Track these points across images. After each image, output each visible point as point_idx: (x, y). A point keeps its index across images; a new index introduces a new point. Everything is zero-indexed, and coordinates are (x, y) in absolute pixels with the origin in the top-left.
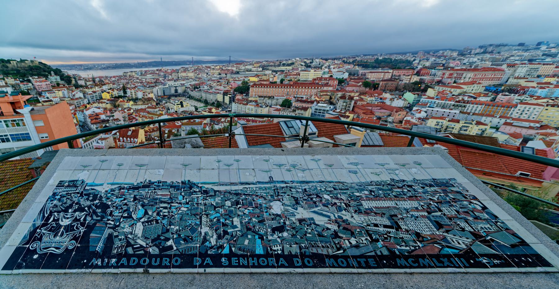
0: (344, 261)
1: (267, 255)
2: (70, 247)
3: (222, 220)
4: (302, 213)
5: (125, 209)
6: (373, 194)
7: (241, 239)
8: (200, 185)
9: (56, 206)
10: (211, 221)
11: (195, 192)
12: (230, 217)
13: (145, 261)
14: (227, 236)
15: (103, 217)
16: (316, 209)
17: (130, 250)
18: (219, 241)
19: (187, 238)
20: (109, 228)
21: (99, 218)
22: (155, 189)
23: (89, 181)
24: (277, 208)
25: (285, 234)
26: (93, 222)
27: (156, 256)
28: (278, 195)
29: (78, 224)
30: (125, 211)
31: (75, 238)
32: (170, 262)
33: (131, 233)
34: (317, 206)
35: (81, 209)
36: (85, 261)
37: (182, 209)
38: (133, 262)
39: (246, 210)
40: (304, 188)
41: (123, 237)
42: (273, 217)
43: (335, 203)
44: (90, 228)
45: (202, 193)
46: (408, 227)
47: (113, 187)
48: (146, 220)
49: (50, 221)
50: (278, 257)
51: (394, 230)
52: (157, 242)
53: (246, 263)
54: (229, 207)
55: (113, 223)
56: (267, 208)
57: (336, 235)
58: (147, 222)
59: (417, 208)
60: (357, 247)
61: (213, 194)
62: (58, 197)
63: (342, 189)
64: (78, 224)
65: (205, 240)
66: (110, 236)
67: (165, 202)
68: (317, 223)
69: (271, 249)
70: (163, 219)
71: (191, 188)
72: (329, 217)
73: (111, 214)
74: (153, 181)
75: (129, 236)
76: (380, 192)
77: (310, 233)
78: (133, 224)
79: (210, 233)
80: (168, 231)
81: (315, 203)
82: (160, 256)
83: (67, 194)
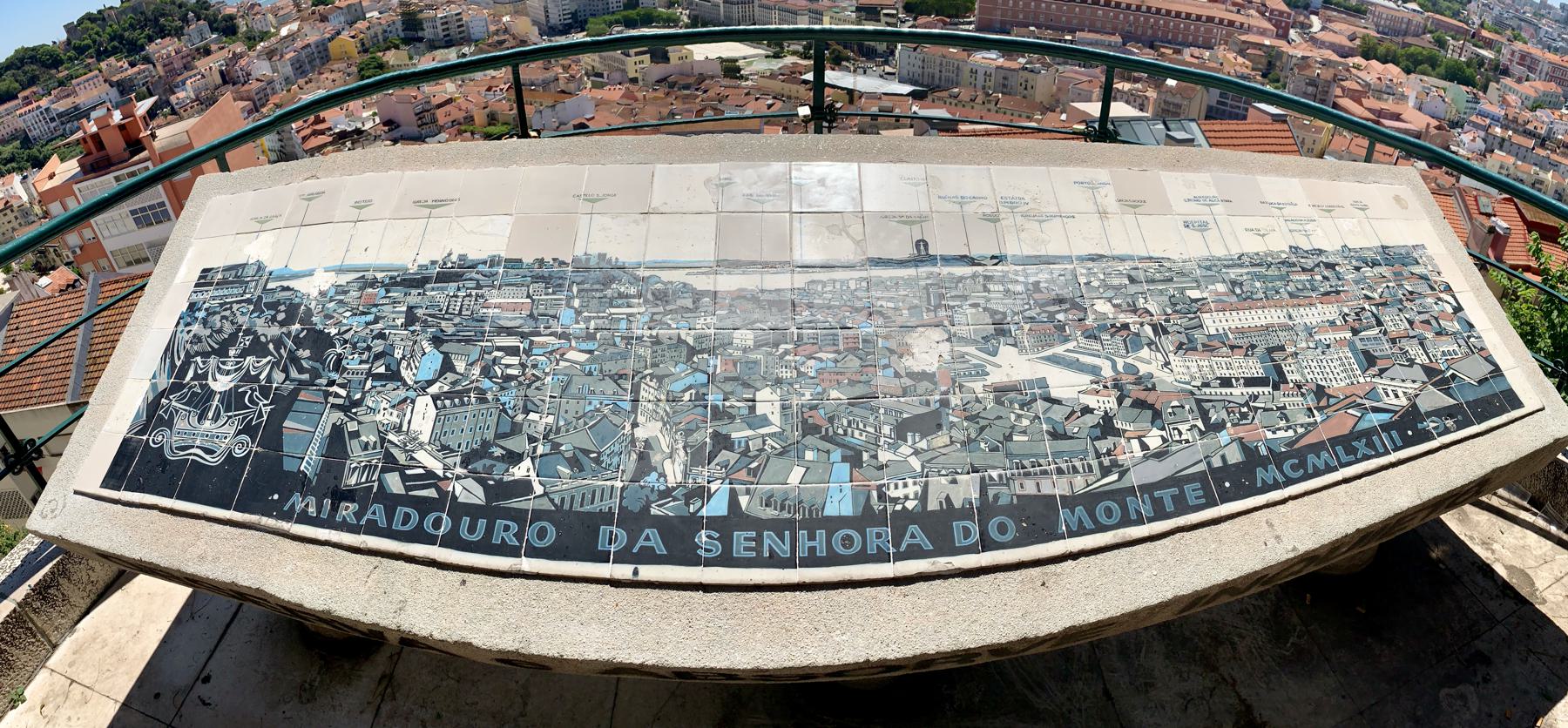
0: (1114, 506)
1: (866, 518)
2: (239, 453)
3: (714, 398)
4: (1013, 365)
5: (380, 349)
6: (1238, 291)
7: (775, 464)
8: (641, 273)
9: (197, 339)
10: (673, 399)
11: (621, 295)
12: (746, 385)
13: (437, 523)
14: (724, 455)
15: (316, 374)
16: (1059, 350)
17: (394, 483)
18: (695, 470)
19: (580, 456)
20: (333, 406)
21: (306, 377)
22: (479, 287)
23: (273, 265)
24: (927, 352)
25: (941, 439)
26: (290, 386)
27: (473, 511)
28: (938, 306)
29: (253, 390)
30: (378, 357)
31: (248, 429)
32: (519, 536)
33: (398, 429)
34: (1066, 340)
35: (257, 348)
36: (276, 497)
37: (572, 355)
38: (404, 524)
39: (811, 363)
40: (1032, 279)
41: (373, 439)
42: (907, 382)
43: (1126, 326)
44: (284, 404)
45: (646, 301)
46: (1303, 375)
47: (343, 279)
48: (446, 388)
49: (188, 378)
50: (903, 519)
51: (1267, 390)
52: (478, 465)
53: (784, 549)
54: (745, 350)
55: (343, 392)
56: (892, 352)
57: (1107, 427)
58: (449, 395)
59: (1332, 323)
60: (1160, 455)
61: (688, 303)
62: (201, 315)
63: (1153, 281)
64: (253, 390)
65: (644, 463)
66: (337, 431)
67: (509, 331)
68: (1054, 394)
69: (882, 497)
70: (503, 389)
71: (607, 282)
72: (1094, 370)
73: (338, 366)
74: (473, 256)
75: (391, 437)
76: (1258, 285)
77: (1024, 432)
78: (405, 400)
79: (664, 441)
80: (516, 429)
81: (1061, 327)
82: (487, 512)
83: (221, 305)
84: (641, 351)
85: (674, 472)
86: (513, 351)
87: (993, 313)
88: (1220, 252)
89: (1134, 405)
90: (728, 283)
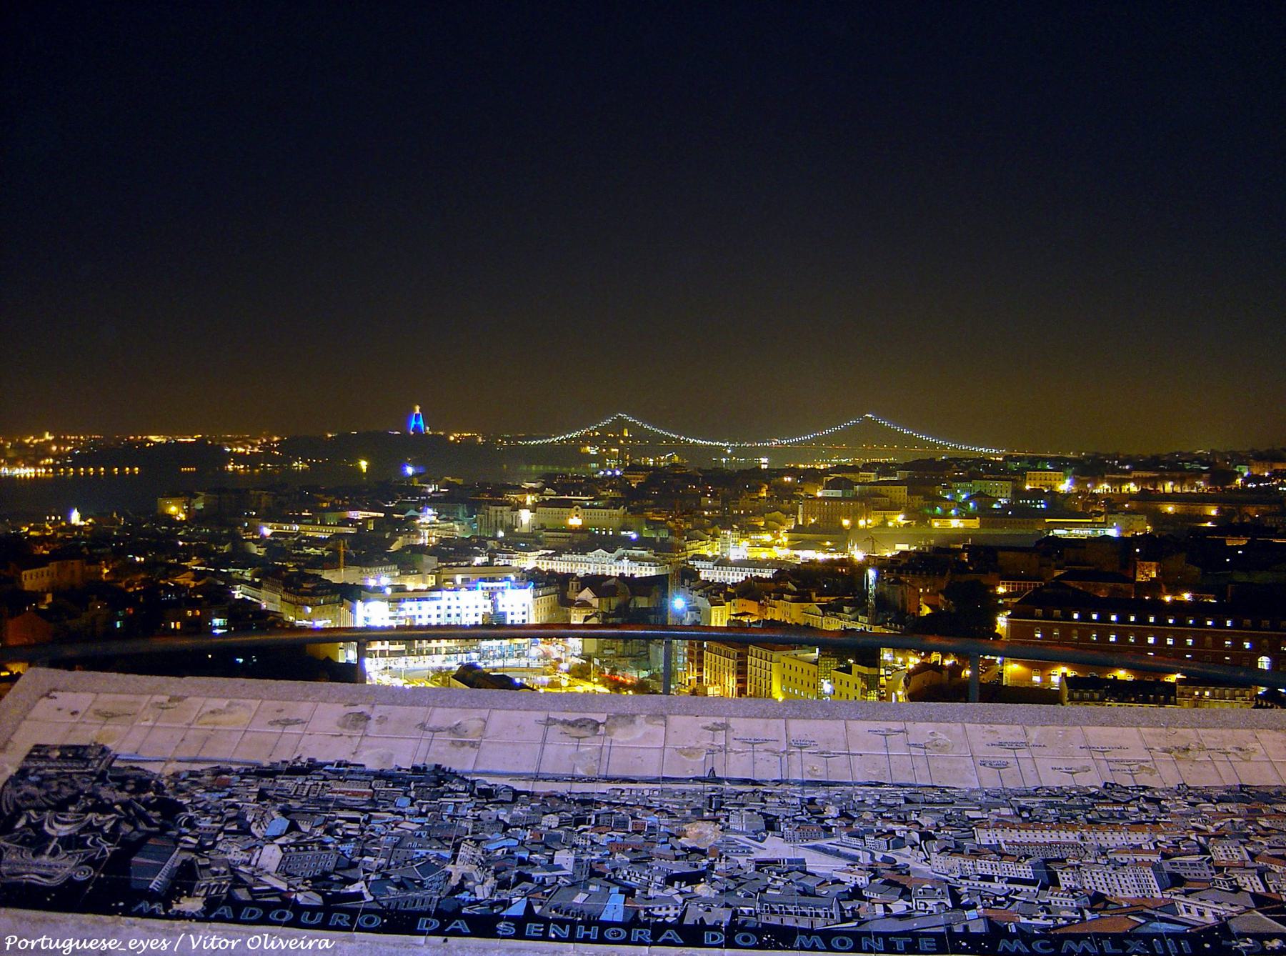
2: (80, 877)
4: (775, 848)
11: (451, 791)
14: (525, 884)
15: (164, 828)
16: (823, 843)
17: (242, 894)
22: (325, 779)
33: (248, 864)
44: (131, 847)
48: (292, 841)
56: (672, 835)
57: (856, 893)
60: (900, 917)
63: (931, 803)
73: (190, 823)
74: (320, 760)
75: (242, 868)
80: (354, 865)
84: (464, 824)
85: (482, 893)
86: (356, 820)
87: (765, 816)
88: (1010, 785)
89: (886, 883)
90: (542, 788)
